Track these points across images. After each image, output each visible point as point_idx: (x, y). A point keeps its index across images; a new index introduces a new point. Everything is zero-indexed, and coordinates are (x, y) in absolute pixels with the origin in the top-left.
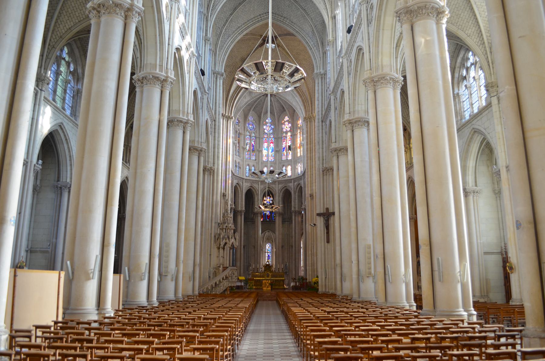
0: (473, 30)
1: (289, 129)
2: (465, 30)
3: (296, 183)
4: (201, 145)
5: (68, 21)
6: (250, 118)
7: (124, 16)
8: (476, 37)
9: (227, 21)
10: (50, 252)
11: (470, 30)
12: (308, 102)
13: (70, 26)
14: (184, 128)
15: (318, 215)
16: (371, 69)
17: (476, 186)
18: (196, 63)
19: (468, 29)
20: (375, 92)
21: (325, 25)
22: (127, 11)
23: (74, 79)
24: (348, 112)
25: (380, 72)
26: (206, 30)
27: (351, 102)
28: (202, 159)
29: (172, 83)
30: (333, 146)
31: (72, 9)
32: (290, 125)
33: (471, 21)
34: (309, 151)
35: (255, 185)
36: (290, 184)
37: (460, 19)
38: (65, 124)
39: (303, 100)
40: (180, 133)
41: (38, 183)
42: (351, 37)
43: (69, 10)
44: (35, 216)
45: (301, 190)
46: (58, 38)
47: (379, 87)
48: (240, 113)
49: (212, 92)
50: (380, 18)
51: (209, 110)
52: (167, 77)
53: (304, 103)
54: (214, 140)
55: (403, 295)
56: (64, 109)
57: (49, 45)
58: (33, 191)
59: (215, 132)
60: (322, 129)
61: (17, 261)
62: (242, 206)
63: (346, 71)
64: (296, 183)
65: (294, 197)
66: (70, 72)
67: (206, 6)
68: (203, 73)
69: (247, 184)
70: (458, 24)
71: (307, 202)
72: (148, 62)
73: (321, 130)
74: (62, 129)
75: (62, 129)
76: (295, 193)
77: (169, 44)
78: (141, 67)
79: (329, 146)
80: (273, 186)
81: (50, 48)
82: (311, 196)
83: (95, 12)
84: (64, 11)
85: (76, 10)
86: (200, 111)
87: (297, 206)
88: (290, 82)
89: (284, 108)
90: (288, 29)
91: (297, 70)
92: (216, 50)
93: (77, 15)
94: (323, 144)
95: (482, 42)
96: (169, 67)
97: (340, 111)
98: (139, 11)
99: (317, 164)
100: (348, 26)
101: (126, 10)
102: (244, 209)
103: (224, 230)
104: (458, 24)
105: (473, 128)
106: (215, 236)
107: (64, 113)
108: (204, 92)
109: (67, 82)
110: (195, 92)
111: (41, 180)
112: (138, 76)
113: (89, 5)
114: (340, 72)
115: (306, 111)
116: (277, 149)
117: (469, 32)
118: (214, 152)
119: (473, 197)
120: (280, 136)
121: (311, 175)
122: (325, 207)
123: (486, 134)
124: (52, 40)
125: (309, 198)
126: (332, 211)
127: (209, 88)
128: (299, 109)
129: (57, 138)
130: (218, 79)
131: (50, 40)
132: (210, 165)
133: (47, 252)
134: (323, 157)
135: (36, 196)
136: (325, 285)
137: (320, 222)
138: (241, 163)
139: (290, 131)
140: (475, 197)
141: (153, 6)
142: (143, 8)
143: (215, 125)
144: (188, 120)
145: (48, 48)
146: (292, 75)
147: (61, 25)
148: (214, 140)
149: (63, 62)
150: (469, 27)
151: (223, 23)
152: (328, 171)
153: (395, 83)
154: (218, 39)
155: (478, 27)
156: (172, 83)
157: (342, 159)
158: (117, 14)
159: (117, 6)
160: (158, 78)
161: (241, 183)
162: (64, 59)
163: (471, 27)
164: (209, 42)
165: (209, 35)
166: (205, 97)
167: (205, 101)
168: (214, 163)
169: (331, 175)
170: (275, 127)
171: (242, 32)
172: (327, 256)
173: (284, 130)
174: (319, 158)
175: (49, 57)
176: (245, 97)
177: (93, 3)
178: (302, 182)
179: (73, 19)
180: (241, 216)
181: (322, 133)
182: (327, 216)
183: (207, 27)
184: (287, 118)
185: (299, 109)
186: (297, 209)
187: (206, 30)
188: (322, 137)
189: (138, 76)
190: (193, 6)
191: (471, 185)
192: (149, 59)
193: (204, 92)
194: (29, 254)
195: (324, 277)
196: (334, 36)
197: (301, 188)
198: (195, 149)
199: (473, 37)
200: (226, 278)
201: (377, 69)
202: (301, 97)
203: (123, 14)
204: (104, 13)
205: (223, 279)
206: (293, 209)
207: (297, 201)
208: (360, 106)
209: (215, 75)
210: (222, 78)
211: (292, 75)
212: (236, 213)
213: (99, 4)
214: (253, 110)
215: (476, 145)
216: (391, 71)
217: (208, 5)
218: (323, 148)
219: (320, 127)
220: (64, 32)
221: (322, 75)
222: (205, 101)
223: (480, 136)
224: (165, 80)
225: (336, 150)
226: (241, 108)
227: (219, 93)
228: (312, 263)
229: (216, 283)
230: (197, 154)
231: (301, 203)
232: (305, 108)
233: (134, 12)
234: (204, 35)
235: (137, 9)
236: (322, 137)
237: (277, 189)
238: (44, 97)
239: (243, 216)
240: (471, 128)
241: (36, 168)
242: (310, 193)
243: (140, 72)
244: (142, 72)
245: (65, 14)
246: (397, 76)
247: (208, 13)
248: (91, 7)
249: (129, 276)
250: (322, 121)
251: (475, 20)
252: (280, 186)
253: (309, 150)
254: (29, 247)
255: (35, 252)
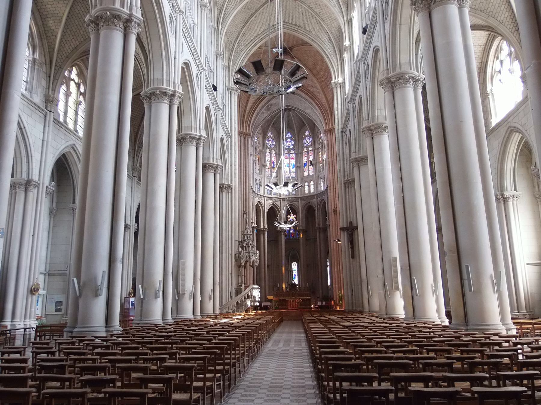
0: (506, 16)
1: (310, 144)
2: (496, 16)
3: (319, 199)
4: (217, 162)
5: (73, 40)
6: (270, 135)
7: (123, 28)
8: (510, 23)
9: (239, 34)
10: (68, 274)
11: (503, 16)
12: (328, 114)
13: (76, 45)
14: (197, 144)
15: (342, 229)
16: (388, 69)
17: (516, 190)
18: (207, 78)
19: (500, 15)
20: (393, 93)
21: (342, 33)
22: (126, 22)
23: (85, 100)
24: (367, 118)
25: (398, 70)
26: (217, 45)
27: (370, 107)
28: (218, 176)
29: (180, 98)
30: (353, 156)
31: (76, 27)
32: (311, 139)
33: (503, 6)
34: (331, 165)
35: (277, 203)
36: (313, 200)
37: (491, 4)
38: (77, 146)
39: (322, 113)
40: (192, 150)
41: (54, 206)
42: (367, 38)
43: (73, 28)
44: (52, 238)
45: (324, 206)
46: (64, 58)
47: (397, 87)
48: (259, 130)
49: (227, 109)
50: (397, 13)
51: (225, 127)
52: (175, 91)
53: (323, 115)
54: (231, 157)
55: (435, 312)
56: (77, 131)
57: (56, 65)
58: (50, 214)
59: (231, 149)
60: (343, 140)
61: (31, 283)
62: (264, 224)
63: (363, 75)
64: (319, 199)
65: (318, 213)
66: (81, 94)
67: (216, 20)
68: (215, 89)
69: (268, 202)
70: (488, 11)
71: (331, 217)
72: (155, 78)
73: (341, 142)
74: (75, 150)
75: (75, 150)
76: (318, 209)
77: (175, 58)
78: (148, 83)
79: (350, 156)
80: (296, 203)
81: (57, 68)
82: (335, 211)
83: (93, 25)
84: (68, 30)
85: (80, 28)
86: (214, 127)
87: (321, 223)
88: (291, 82)
89: (303, 122)
90: (303, 38)
91: (298, 68)
92: (229, 65)
93: (82, 33)
94: (343, 156)
95: (517, 29)
96: (176, 82)
97: (360, 119)
98: (139, 22)
99: (339, 177)
100: (364, 26)
101: (125, 21)
102: (266, 227)
103: (245, 248)
104: (488, 11)
105: (510, 127)
106: (235, 255)
107: (76, 135)
108: (217, 108)
109: (78, 104)
110: (207, 108)
111: (57, 203)
112: (145, 92)
113: (87, 18)
114: (357, 77)
115: (326, 124)
116: (298, 165)
117: (502, 19)
118: (231, 169)
119: (513, 202)
120: (301, 151)
121: (334, 189)
122: (349, 221)
123: (524, 131)
124: (59, 61)
125: (333, 214)
126: (355, 225)
127: (224, 105)
128: (319, 122)
129: (70, 159)
130: (233, 95)
131: (56, 61)
132: (228, 182)
133: (65, 274)
134: (344, 169)
135: (52, 219)
136: (352, 303)
137: (344, 237)
138: (262, 181)
139: (311, 145)
140: (515, 203)
141: (156, 19)
142: (143, 19)
143: (231, 142)
144: (201, 136)
145: (55, 69)
146: (292, 74)
147: (66, 45)
148: (231, 157)
149: (72, 83)
150: (501, 12)
151: (235, 37)
152: (349, 183)
153: (416, 81)
154: (231, 54)
155: (511, 11)
156: (180, 98)
157: (363, 169)
158: (116, 26)
159: (115, 18)
160: (165, 92)
161: (263, 201)
162: (74, 80)
163: (504, 13)
164: (221, 57)
165: (221, 49)
166: (219, 113)
167: (219, 117)
168: (231, 181)
169: (353, 188)
170: (295, 142)
171: (255, 45)
172: (352, 272)
173: (305, 145)
174: (340, 170)
175: (57, 77)
176: (263, 113)
177: (91, 16)
178: (325, 197)
179: (78, 38)
180: (264, 235)
181: (343, 144)
182: (351, 230)
183: (217, 41)
184: (307, 133)
185: (319, 122)
186: (321, 226)
187: (217, 45)
188: (343, 148)
189: (145, 92)
190: (201, 19)
191: (509, 189)
192: (155, 75)
193: (217, 108)
194: (47, 277)
195: (350, 294)
196: (351, 40)
197: (325, 203)
198: (210, 166)
199: (507, 23)
200: (248, 297)
201: (394, 69)
202: (320, 109)
203: (121, 26)
204: (102, 26)
205: (245, 298)
206: (317, 226)
207: (321, 217)
208: (379, 111)
209: (230, 91)
210: (237, 94)
211: (292, 74)
212: (259, 232)
213: (97, 16)
214: (272, 126)
215: (513, 145)
216: (411, 69)
217: (218, 19)
218: (343, 160)
219: (340, 138)
220: (70, 51)
221: (340, 84)
222: (219, 117)
223: (517, 134)
224: (173, 95)
225: (356, 160)
226: (259, 125)
227: (234, 109)
228: (338, 281)
229: (238, 303)
230: (213, 171)
231: (325, 220)
232: (325, 120)
233: (133, 23)
234: (215, 49)
235: (135, 20)
236: (343, 148)
237: (300, 205)
238: (54, 118)
239: (266, 234)
240: (508, 126)
241: (48, 190)
242: (333, 208)
243: (147, 87)
244: (149, 88)
245: (69, 33)
246: (417, 74)
247: (218, 27)
248: (89, 20)
249: (144, 294)
250: (342, 132)
251: (507, 4)
252: (303, 202)
253: (331, 163)
254: (47, 270)
255: (53, 275)
